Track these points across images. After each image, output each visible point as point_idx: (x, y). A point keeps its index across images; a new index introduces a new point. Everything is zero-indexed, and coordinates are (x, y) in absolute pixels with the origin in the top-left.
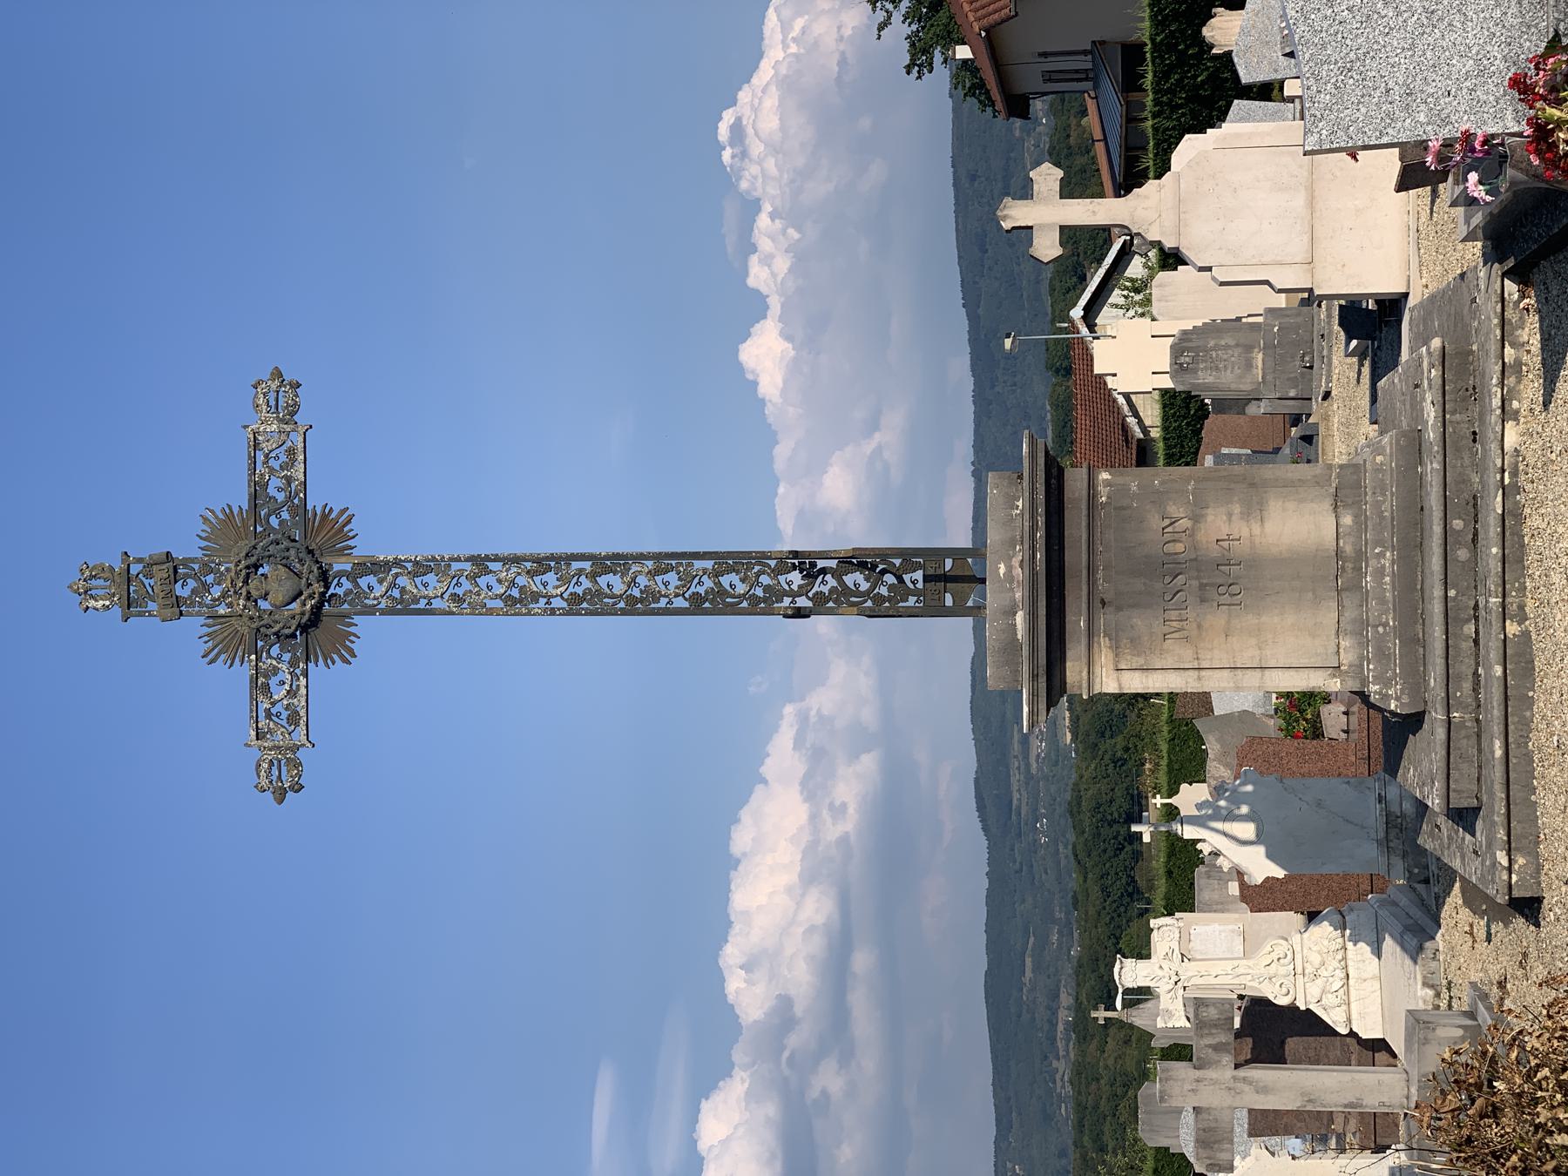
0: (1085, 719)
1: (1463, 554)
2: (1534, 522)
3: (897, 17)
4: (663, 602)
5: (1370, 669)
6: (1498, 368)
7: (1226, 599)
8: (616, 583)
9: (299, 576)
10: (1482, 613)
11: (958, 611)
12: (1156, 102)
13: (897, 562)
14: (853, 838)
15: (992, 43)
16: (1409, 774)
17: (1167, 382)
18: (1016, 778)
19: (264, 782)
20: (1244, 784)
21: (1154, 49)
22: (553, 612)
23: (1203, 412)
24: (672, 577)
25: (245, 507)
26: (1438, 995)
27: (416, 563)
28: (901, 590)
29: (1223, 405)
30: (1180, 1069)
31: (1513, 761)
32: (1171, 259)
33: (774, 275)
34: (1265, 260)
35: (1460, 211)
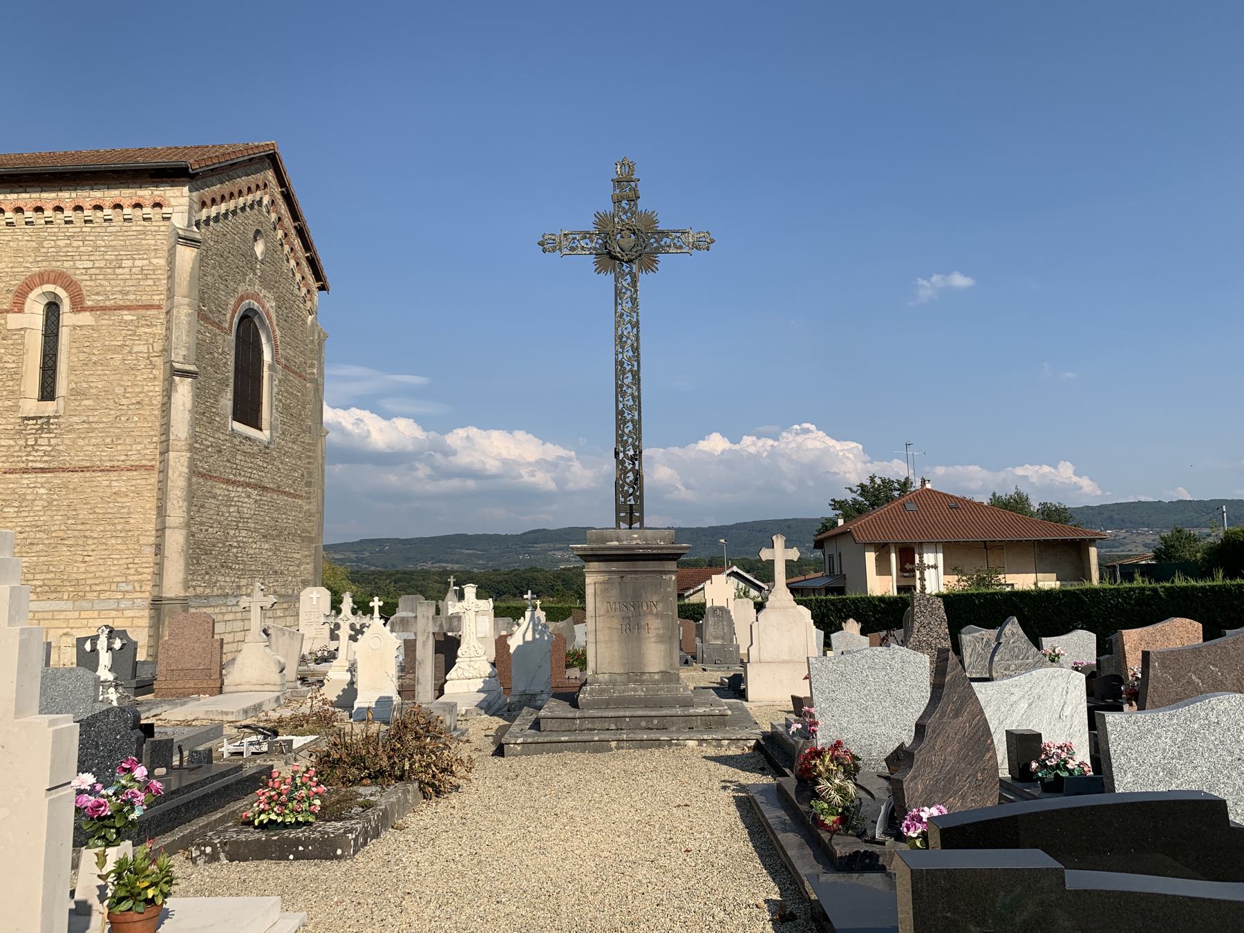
0: (570, 573)
1: (643, 724)
2: (657, 753)
3: (854, 495)
4: (621, 399)
5: (596, 686)
6: (720, 738)
7: (624, 627)
8: (628, 380)
9: (631, 251)
10: (619, 732)
11: (618, 519)
12: (822, 600)
13: (638, 494)
14: (521, 480)
15: (845, 534)
16: (553, 703)
17: (709, 605)
18: (546, 545)
19: (546, 237)
20: (548, 636)
21: (844, 600)
22: (616, 354)
23: (697, 620)
24: (631, 403)
25: (658, 229)
26: (463, 716)
27: (636, 299)
28: (626, 495)
29: (699, 629)
30: (432, 611)
31: (560, 745)
32: (759, 607)
33: (748, 446)
34: (761, 644)
35: (783, 722)
